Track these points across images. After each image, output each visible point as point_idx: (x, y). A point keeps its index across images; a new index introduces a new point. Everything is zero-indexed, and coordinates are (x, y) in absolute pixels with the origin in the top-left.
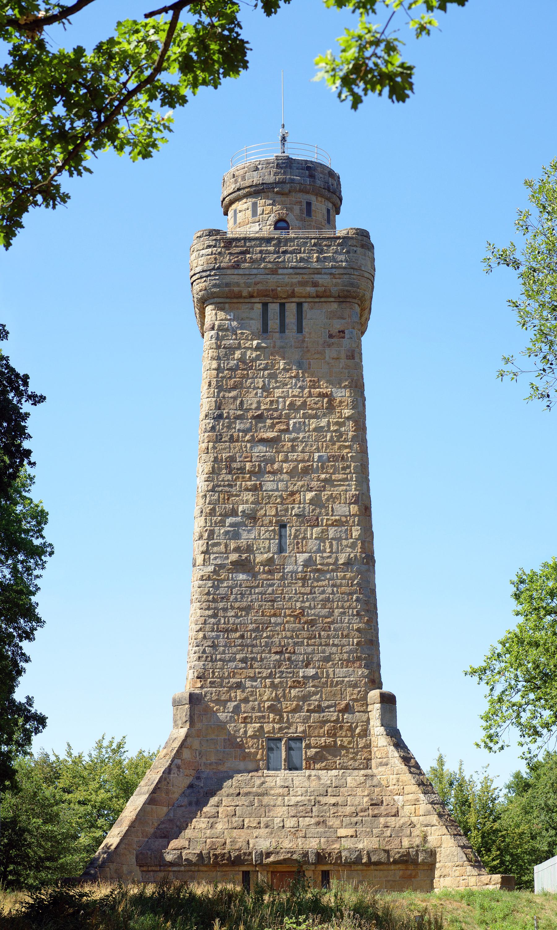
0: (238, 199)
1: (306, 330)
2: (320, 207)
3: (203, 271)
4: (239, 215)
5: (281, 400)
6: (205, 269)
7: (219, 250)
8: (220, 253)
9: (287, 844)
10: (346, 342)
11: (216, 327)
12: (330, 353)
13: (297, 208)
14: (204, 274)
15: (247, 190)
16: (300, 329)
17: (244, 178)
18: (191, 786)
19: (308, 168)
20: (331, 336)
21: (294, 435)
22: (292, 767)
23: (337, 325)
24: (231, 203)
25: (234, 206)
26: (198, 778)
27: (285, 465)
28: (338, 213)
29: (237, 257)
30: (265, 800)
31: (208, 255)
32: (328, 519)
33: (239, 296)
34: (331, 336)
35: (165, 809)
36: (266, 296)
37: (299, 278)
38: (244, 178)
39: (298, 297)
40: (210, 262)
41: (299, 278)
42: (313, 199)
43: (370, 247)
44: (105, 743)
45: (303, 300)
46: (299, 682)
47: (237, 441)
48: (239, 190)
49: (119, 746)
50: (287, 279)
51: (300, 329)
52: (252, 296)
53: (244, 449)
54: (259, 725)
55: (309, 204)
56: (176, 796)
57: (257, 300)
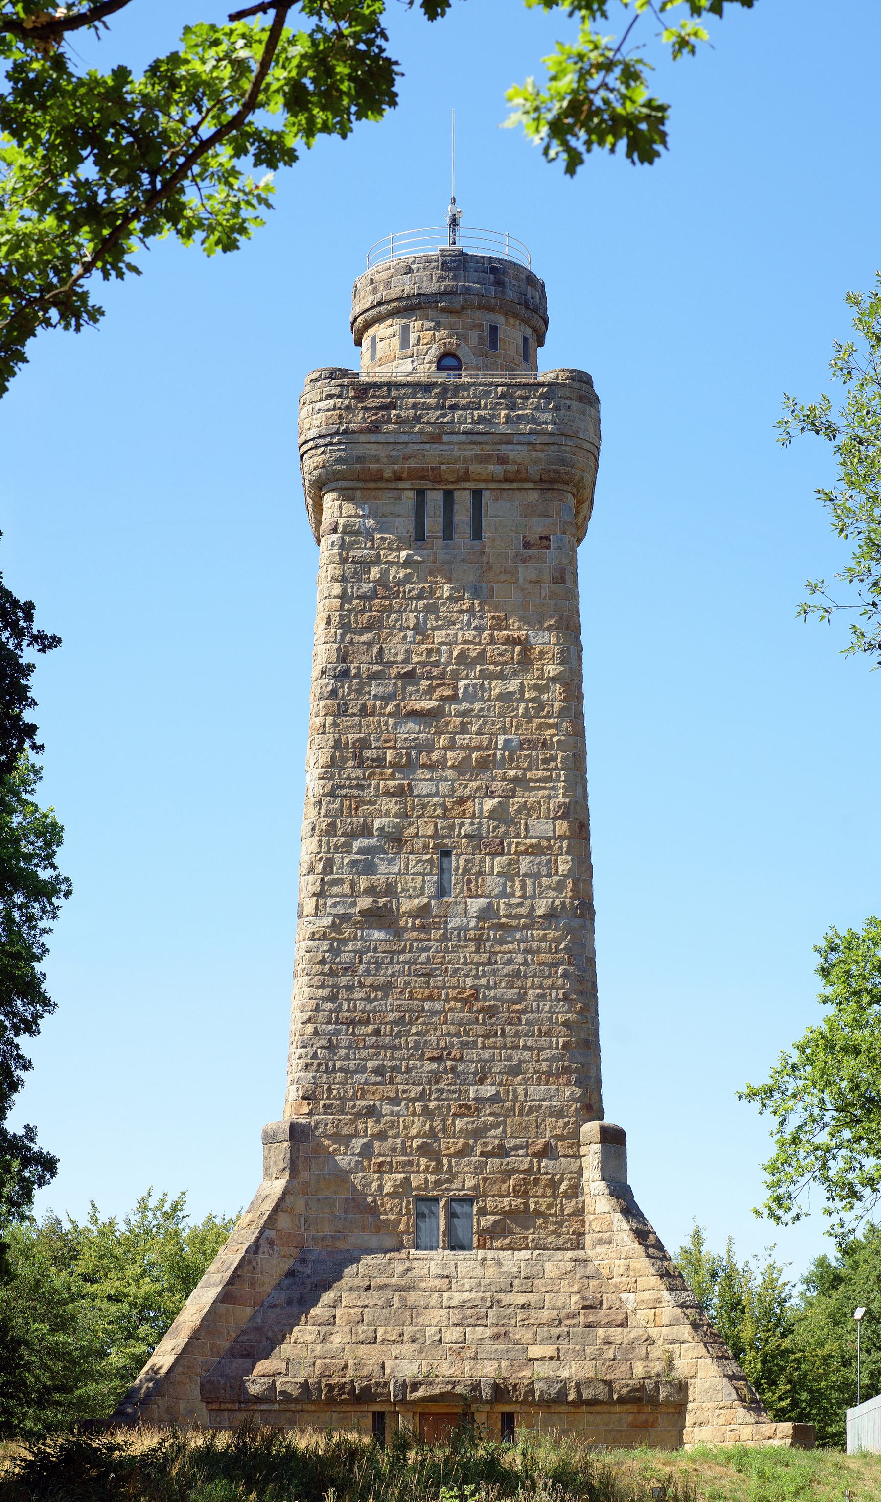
0: (378, 319)
1: (486, 534)
2: (512, 333)
3: (320, 437)
4: (379, 346)
5: (444, 648)
6: (323, 432)
7: (347, 402)
8: (348, 408)
9: (446, 1369)
10: (551, 555)
11: (340, 528)
12: (525, 573)
13: (474, 335)
14: (322, 441)
15: (393, 305)
16: (477, 534)
17: (388, 286)
18: (291, 1274)
19: (494, 270)
20: (527, 545)
21: (465, 706)
22: (455, 1245)
23: (538, 527)
24: (368, 325)
25: (371, 331)
26: (303, 1261)
27: (450, 754)
28: (541, 343)
29: (377, 414)
30: (412, 1297)
31: (329, 410)
32: (518, 844)
33: (378, 477)
34: (527, 545)
35: (249, 1311)
36: (423, 478)
37: (477, 450)
38: (388, 286)
39: (475, 480)
40: (331, 421)
41: (477, 450)
42: (500, 320)
43: (593, 401)
44: (153, 1203)
45: (482, 485)
46: (468, 1107)
47: (373, 714)
48: (380, 304)
49: (176, 1207)
50: (456, 451)
51: (477, 534)
52: (399, 479)
53: (384, 728)
54: (403, 1175)
55: (494, 329)
56: (267, 1288)
57: (407, 485)
